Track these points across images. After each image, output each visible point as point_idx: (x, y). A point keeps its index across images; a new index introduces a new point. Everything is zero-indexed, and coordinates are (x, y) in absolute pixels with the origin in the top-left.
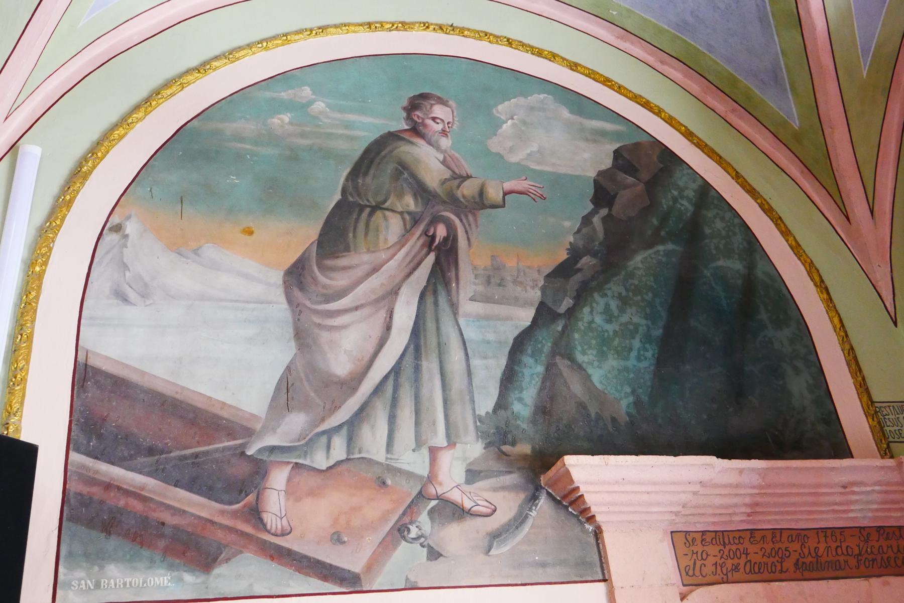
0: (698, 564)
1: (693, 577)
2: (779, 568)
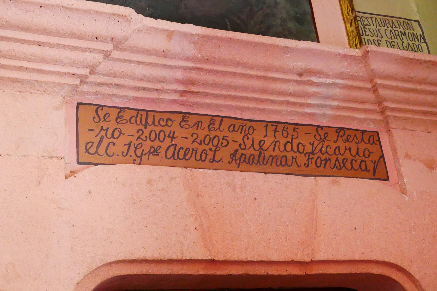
0: (106, 142)
1: (90, 153)
2: (210, 156)
